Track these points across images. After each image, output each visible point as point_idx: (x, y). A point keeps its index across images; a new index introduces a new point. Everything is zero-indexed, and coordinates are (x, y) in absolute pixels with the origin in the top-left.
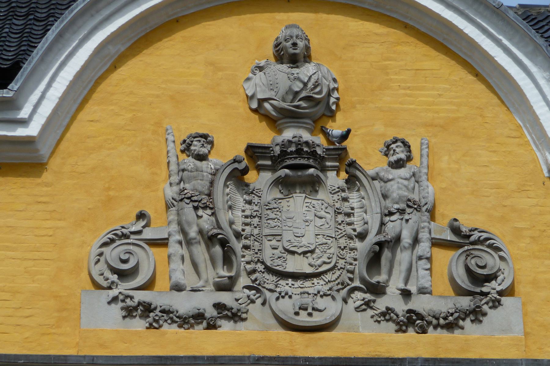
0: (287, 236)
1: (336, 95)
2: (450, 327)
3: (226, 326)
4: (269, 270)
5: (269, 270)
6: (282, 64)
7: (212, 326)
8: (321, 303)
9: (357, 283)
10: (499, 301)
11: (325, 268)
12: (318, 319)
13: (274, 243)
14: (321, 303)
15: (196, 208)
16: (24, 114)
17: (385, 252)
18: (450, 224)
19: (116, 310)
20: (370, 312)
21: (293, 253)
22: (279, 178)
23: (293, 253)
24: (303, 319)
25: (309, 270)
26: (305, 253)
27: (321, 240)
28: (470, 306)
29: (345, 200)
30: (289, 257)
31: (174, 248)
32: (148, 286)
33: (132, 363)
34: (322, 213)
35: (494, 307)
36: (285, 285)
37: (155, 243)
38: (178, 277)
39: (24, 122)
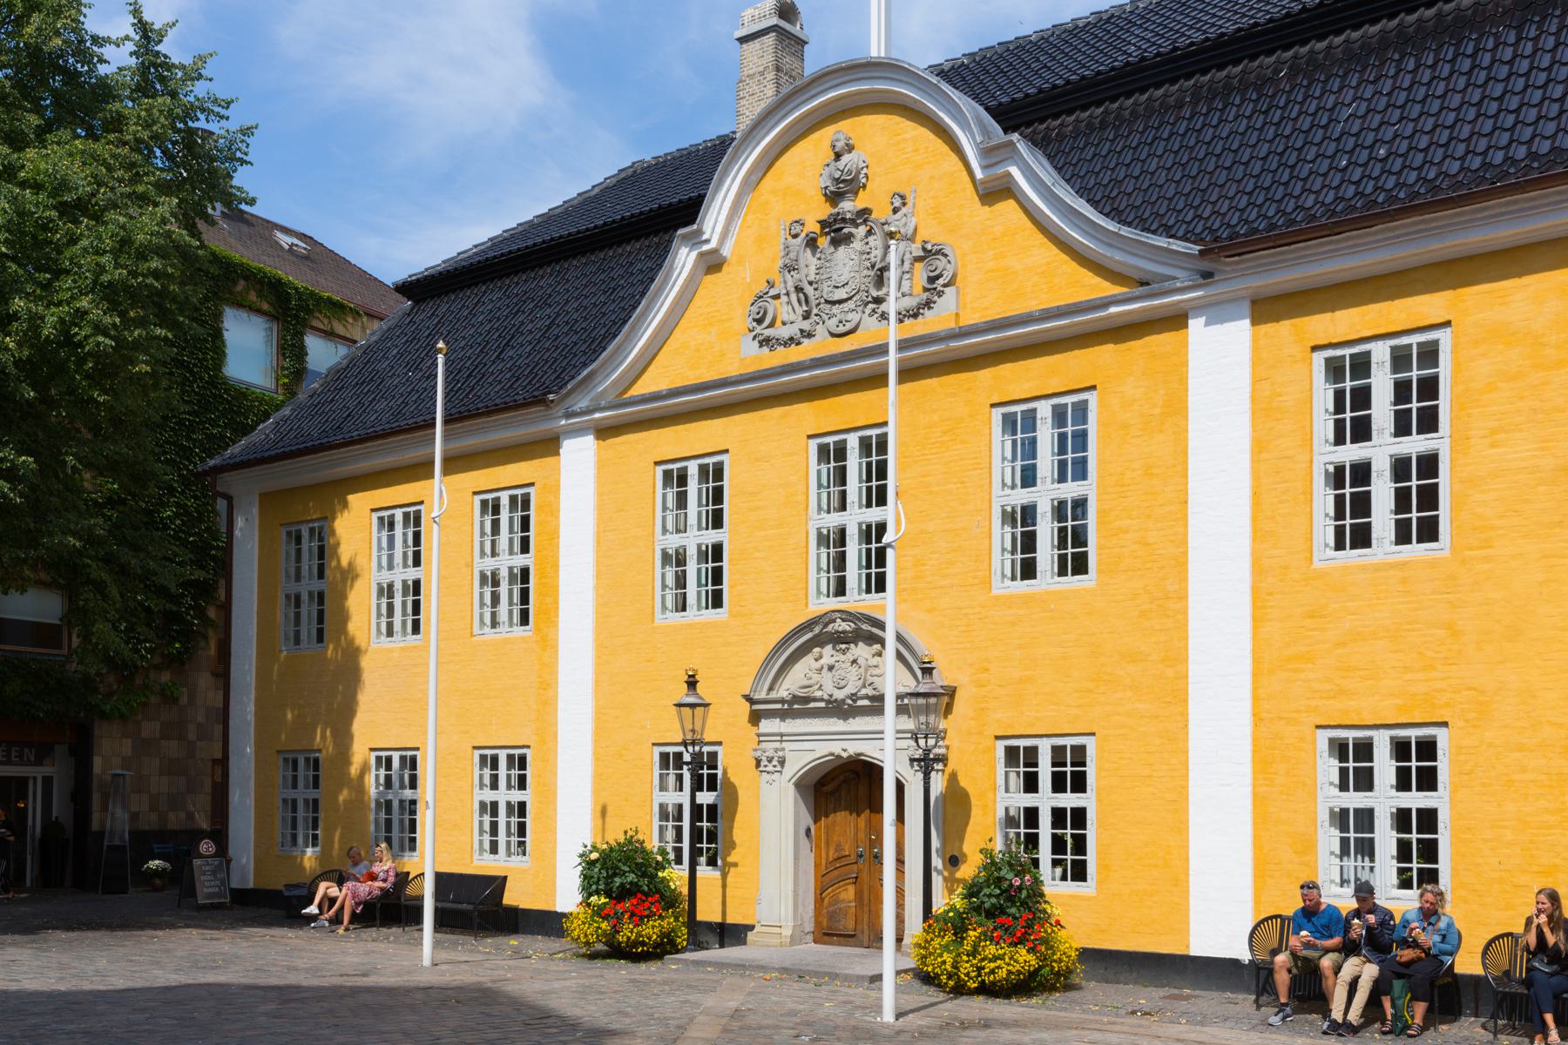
0: (835, 276)
1: (865, 170)
2: (915, 316)
3: (806, 341)
4: (827, 302)
5: (827, 302)
6: (1450, 776)
7: (799, 344)
8: (850, 316)
9: (870, 299)
10: (943, 292)
11: (854, 292)
12: (849, 326)
13: (829, 283)
14: (850, 316)
15: (789, 271)
16: (705, 237)
17: (27, 986)
18: (591, 864)
19: (756, 343)
20: (876, 316)
21: (837, 287)
22: (1101, 249)
23: (837, 287)
24: (842, 329)
25: (845, 296)
26: (843, 286)
27: (853, 274)
28: (990, 840)
29: (867, 243)
30: (836, 290)
31: (784, 299)
32: (771, 325)
33: (469, 614)
34: (853, 257)
35: (940, 296)
36: (836, 309)
37: (777, 297)
38: (786, 318)
39: (707, 241)
